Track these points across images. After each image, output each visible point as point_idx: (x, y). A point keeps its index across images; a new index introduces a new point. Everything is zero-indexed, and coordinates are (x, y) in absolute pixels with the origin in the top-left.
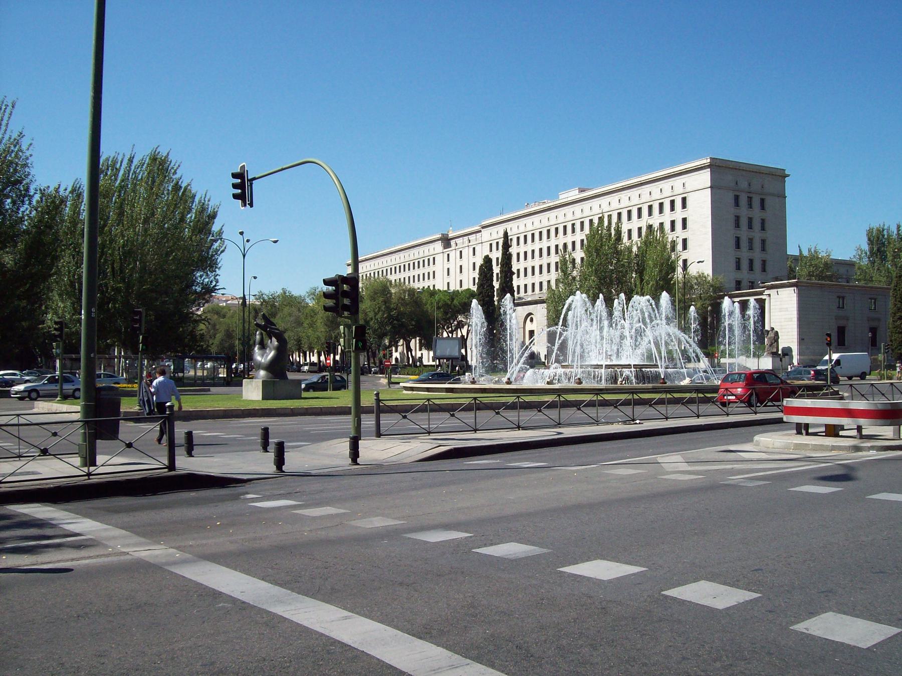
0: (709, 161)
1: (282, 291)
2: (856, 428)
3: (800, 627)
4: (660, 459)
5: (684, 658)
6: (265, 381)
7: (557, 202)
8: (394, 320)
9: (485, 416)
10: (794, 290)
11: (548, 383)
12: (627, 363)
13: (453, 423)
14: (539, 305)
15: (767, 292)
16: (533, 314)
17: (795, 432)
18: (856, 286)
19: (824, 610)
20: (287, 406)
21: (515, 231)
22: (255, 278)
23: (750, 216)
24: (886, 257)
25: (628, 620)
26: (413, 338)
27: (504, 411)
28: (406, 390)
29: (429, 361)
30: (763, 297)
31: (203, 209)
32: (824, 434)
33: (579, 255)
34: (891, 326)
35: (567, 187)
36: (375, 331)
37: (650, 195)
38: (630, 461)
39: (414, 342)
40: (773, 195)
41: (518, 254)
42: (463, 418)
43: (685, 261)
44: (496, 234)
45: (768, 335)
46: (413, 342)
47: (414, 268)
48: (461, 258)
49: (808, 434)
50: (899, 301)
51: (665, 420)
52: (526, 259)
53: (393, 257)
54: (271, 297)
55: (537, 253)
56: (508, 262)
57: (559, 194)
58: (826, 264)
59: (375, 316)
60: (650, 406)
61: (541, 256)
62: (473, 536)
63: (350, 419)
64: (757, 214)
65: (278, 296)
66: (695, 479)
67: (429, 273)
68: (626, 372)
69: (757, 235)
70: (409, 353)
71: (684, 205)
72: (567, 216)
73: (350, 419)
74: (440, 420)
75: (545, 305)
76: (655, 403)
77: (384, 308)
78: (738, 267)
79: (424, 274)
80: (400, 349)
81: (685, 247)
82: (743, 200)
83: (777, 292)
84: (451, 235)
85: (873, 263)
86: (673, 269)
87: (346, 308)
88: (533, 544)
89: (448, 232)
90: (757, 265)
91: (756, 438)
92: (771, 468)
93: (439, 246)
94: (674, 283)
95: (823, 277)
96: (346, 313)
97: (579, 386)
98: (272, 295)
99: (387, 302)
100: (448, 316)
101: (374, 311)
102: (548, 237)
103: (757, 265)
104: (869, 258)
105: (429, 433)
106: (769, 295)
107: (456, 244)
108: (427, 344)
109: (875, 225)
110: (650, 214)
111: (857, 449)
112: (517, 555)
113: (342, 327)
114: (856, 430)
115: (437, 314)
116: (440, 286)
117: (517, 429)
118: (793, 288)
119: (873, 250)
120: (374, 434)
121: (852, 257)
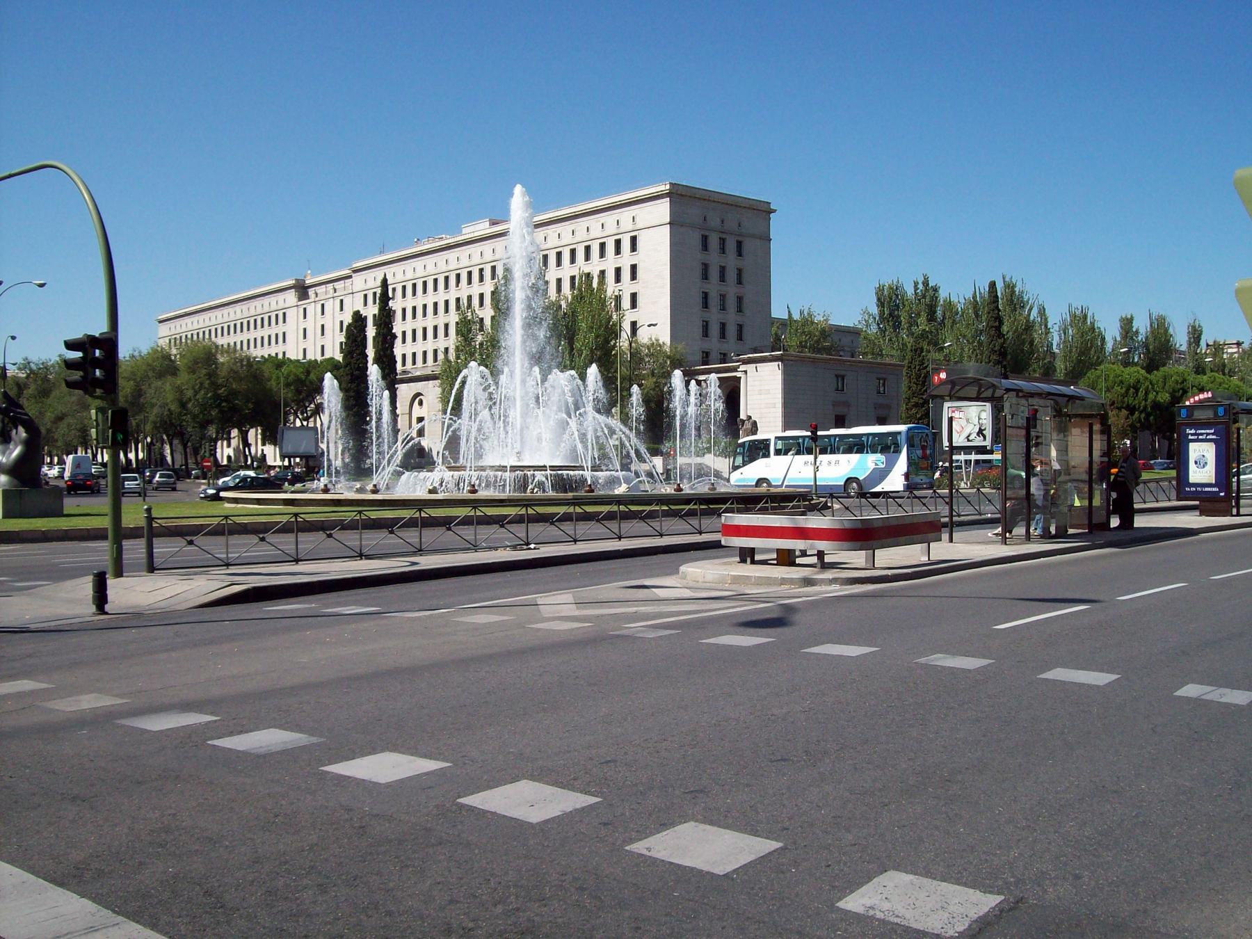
1: (58, 359)
2: (816, 553)
3: (639, 847)
4: (541, 599)
5: (451, 902)
6: (7, 490)
7: (459, 238)
8: (222, 401)
9: (309, 541)
10: (779, 365)
11: (430, 492)
12: (542, 465)
13: (264, 550)
14: (431, 382)
15: (742, 368)
16: (422, 395)
17: (738, 559)
18: (860, 362)
19: (684, 819)
20: (38, 527)
21: (400, 277)
22: (13, 338)
23: (723, 265)
24: (900, 323)
25: (392, 844)
26: (252, 428)
27: (398, 530)
28: (228, 502)
29: (275, 461)
30: (738, 374)
32: (775, 562)
34: (903, 415)
35: (473, 218)
36: (195, 417)
37: (588, 231)
38: (498, 603)
39: (254, 433)
40: (753, 236)
41: (404, 310)
42: (280, 543)
43: (634, 324)
44: (371, 281)
45: (743, 426)
46: (252, 433)
47: (255, 328)
48: (323, 313)
49: (753, 562)
50: (914, 383)
51: (573, 543)
52: (414, 316)
53: (225, 311)
54: (42, 366)
55: (430, 309)
56: (387, 320)
57: (463, 226)
58: (823, 332)
59: (195, 395)
60: (552, 523)
61: (436, 313)
62: (219, 720)
63: (107, 546)
64: (731, 261)
65: (53, 366)
66: (578, 628)
67: (277, 335)
68: (539, 476)
69: (732, 290)
70: (247, 449)
71: (634, 248)
72: (472, 258)
73: (105, 545)
74: (243, 546)
75: (437, 382)
76: (559, 520)
77: (209, 384)
78: (706, 333)
79: (270, 336)
80: (234, 442)
81: (634, 304)
83: (756, 367)
84: (308, 282)
85: (883, 331)
86: (616, 336)
87: (97, 383)
88: (301, 731)
89: (305, 277)
90: (732, 331)
91: (683, 568)
92: (690, 611)
93: (291, 297)
94: (616, 355)
95: (820, 349)
96: (99, 392)
97: (472, 496)
98: (43, 364)
99: (211, 375)
100: (301, 397)
101: (193, 388)
102: (447, 287)
103: (732, 331)
104: (878, 324)
105: (228, 565)
106: (746, 372)
108: (271, 437)
109: (887, 281)
110: (587, 258)
111: (808, 582)
112: (270, 748)
113: (93, 412)
114: (816, 557)
115: (285, 394)
116: (294, 354)
117: (359, 558)
118: (777, 363)
119: (884, 314)
120: (145, 567)
121: (857, 323)
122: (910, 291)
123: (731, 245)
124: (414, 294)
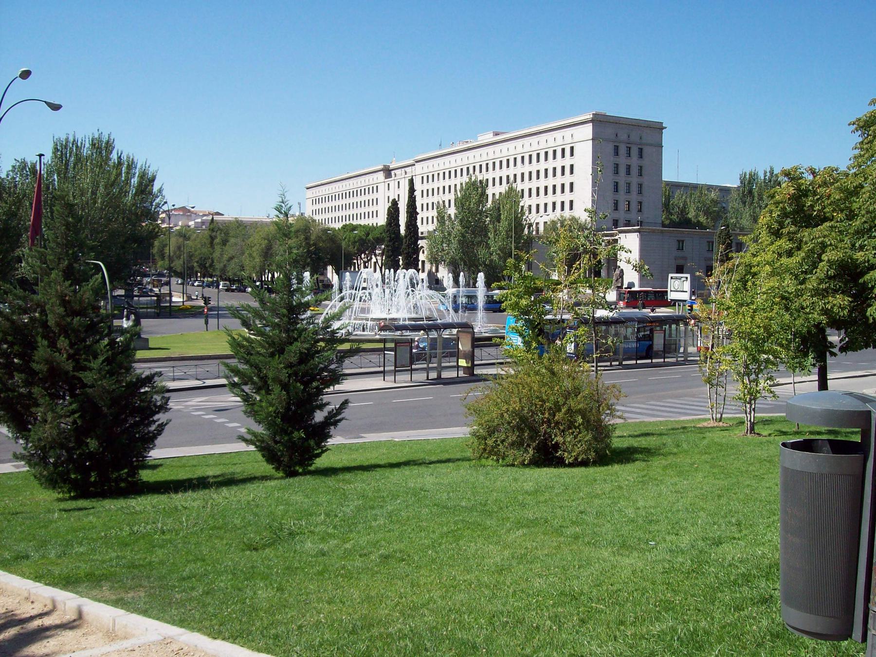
0: (591, 116)
31: (143, 175)
33: (452, 211)
40: (651, 145)
52: (546, 176)
71: (572, 154)
82: (623, 150)
84: (392, 167)
93: (381, 176)
99: (307, 238)
107: (395, 174)
122: (761, 176)
123: (635, 151)
124: (508, 166)
